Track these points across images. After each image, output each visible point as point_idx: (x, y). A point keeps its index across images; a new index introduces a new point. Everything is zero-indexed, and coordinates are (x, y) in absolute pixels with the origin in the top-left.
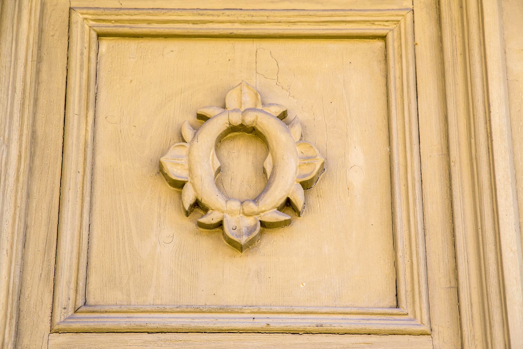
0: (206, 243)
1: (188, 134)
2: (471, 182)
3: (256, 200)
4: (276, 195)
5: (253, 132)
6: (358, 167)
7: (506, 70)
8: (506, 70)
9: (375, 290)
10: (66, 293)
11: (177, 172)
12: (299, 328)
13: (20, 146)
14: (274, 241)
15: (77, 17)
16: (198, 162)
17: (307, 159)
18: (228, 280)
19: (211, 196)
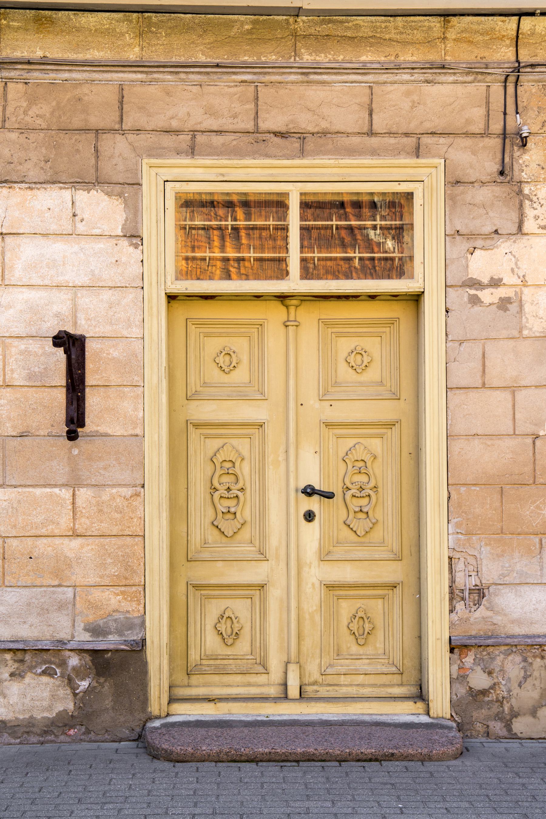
0: (222, 372)
1: (219, 355)
2: (179, 703)
3: (229, 366)
4: (232, 365)
5: (229, 354)
6: (245, 358)
7: (268, 345)
8: (268, 345)
9: (247, 380)
10: (202, 382)
11: (217, 362)
12: (199, 695)
13: (155, 72)
14: (232, 372)
15: (201, 334)
16: (221, 360)
17: (237, 360)
18: (225, 378)
19: (223, 366)
